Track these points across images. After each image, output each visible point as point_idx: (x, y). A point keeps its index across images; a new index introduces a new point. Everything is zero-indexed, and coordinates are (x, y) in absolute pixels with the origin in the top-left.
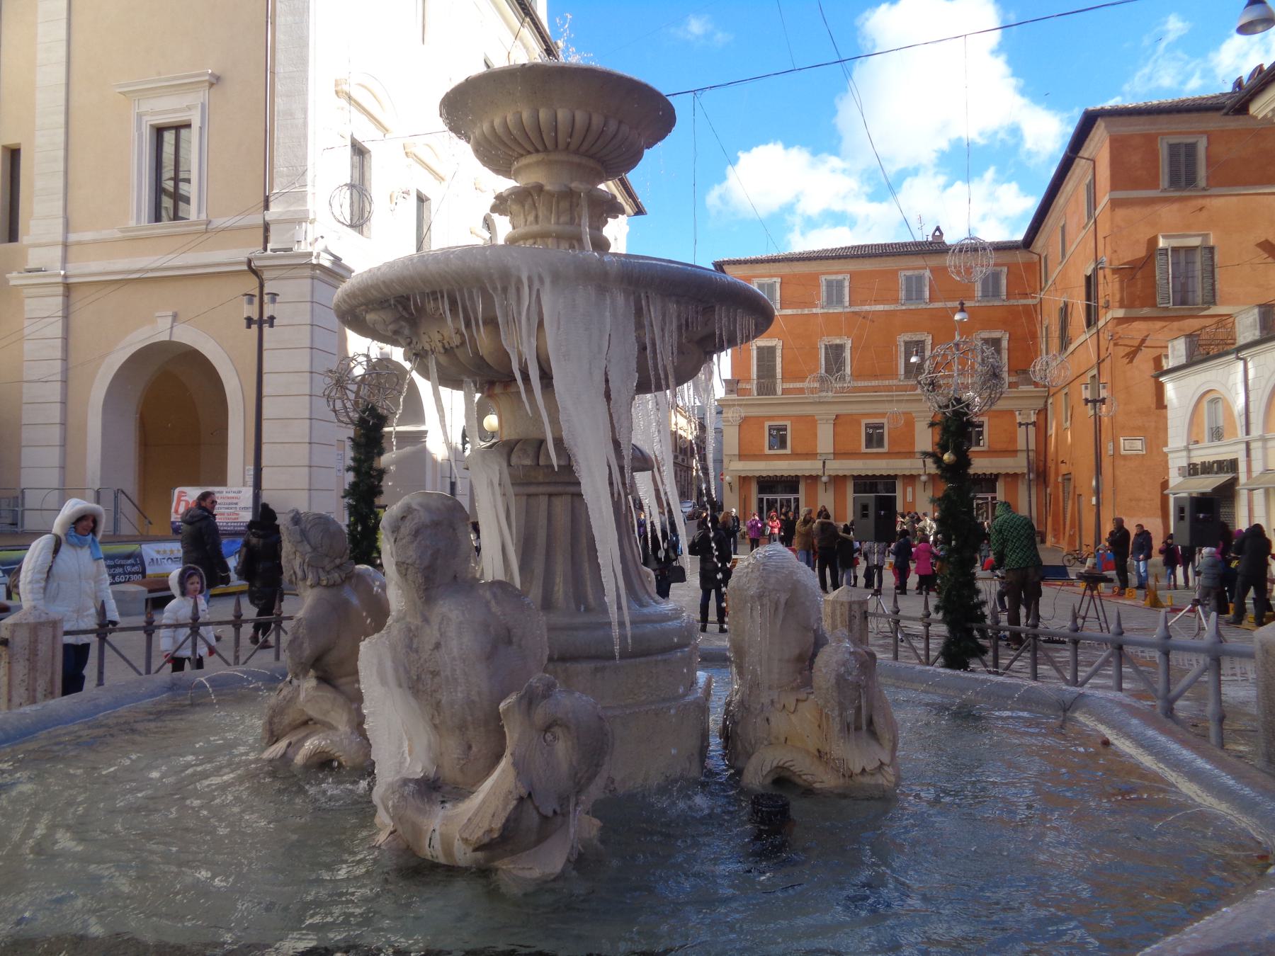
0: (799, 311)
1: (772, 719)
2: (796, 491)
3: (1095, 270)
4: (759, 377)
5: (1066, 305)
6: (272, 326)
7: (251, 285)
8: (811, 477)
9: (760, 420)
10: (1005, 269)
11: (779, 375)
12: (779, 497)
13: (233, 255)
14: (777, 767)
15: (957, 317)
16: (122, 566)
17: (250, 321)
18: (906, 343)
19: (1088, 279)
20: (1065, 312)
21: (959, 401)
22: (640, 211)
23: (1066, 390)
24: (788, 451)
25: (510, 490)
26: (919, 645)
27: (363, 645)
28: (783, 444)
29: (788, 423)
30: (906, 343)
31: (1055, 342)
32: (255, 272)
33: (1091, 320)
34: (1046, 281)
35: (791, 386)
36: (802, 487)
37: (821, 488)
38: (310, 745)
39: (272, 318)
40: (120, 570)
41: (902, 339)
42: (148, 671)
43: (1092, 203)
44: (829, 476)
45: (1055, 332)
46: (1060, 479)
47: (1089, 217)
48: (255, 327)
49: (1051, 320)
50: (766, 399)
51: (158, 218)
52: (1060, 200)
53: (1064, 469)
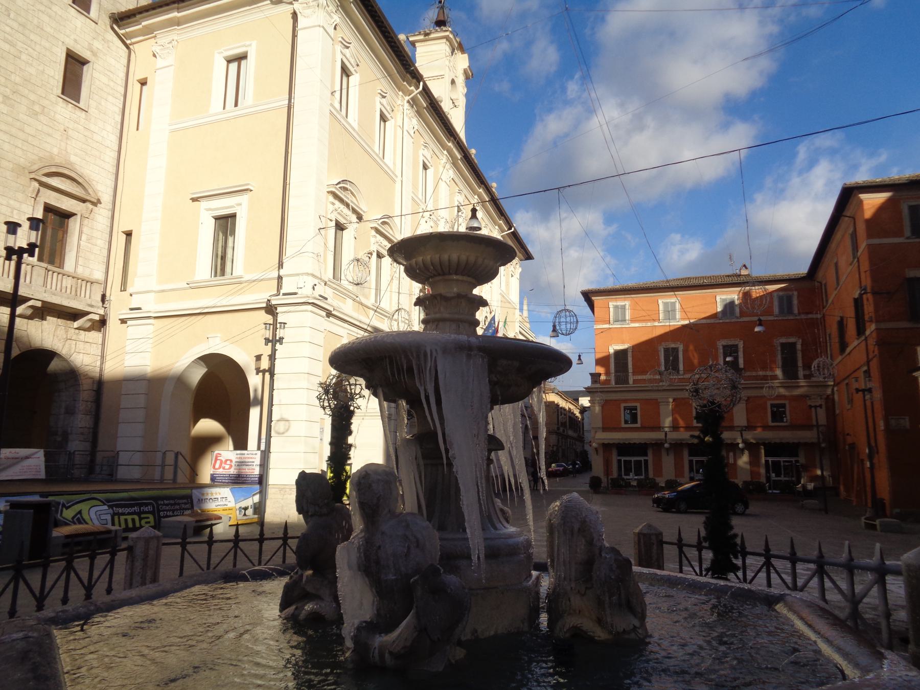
0: (644, 324)
1: (572, 599)
2: (646, 455)
3: (861, 295)
4: (616, 371)
5: (842, 318)
6: (281, 344)
7: (269, 319)
8: (656, 444)
9: (617, 402)
10: (795, 293)
11: (630, 370)
12: (633, 459)
13: (260, 296)
14: (573, 627)
15: (757, 329)
16: (179, 504)
17: (267, 341)
18: (724, 347)
19: (856, 300)
20: (841, 324)
21: (713, 403)
22: (528, 257)
23: (846, 381)
24: (638, 425)
25: (422, 462)
26: (740, 574)
27: (339, 548)
28: (634, 419)
29: (638, 405)
30: (724, 347)
31: (836, 346)
32: (270, 309)
33: (860, 331)
34: (827, 301)
35: (640, 377)
36: (650, 453)
37: (664, 453)
38: (309, 607)
39: (281, 339)
40: (178, 507)
41: (721, 344)
42: (208, 568)
43: (855, 247)
44: (670, 444)
45: (835, 339)
46: (847, 447)
47: (854, 258)
48: (270, 344)
49: (833, 330)
50: (622, 387)
51: (216, 276)
52: (833, 245)
53: (849, 440)
